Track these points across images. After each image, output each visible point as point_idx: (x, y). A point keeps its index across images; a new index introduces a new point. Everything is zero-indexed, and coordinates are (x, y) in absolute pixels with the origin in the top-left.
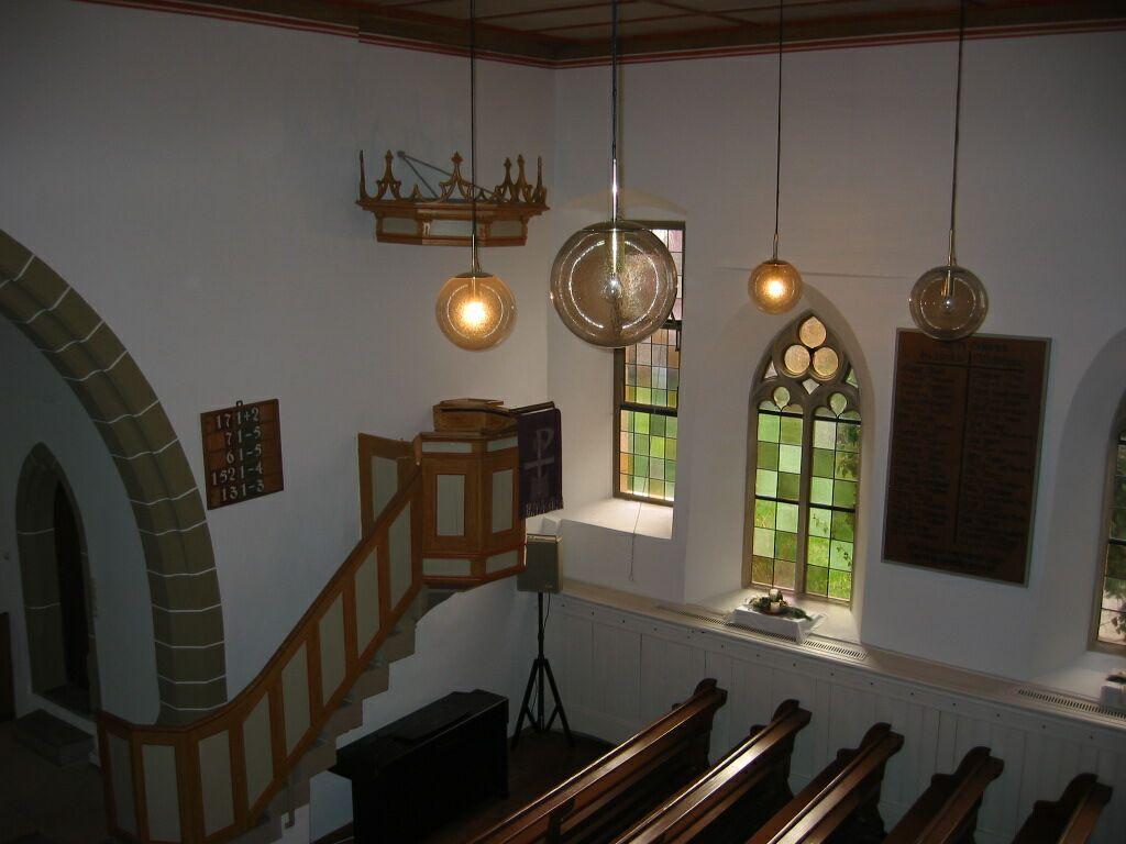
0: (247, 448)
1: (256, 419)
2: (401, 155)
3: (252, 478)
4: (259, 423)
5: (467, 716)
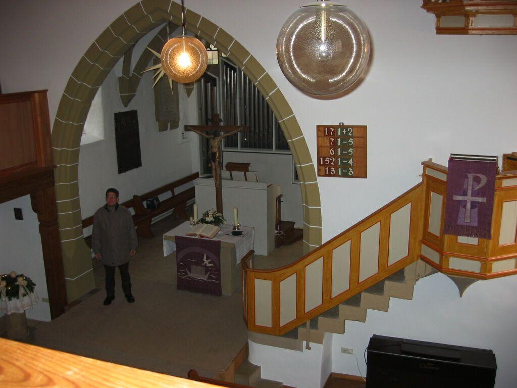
0: (345, 151)
1: (350, 134)
2: (331, 302)
3: (346, 166)
4: (352, 137)
5: (458, 360)
